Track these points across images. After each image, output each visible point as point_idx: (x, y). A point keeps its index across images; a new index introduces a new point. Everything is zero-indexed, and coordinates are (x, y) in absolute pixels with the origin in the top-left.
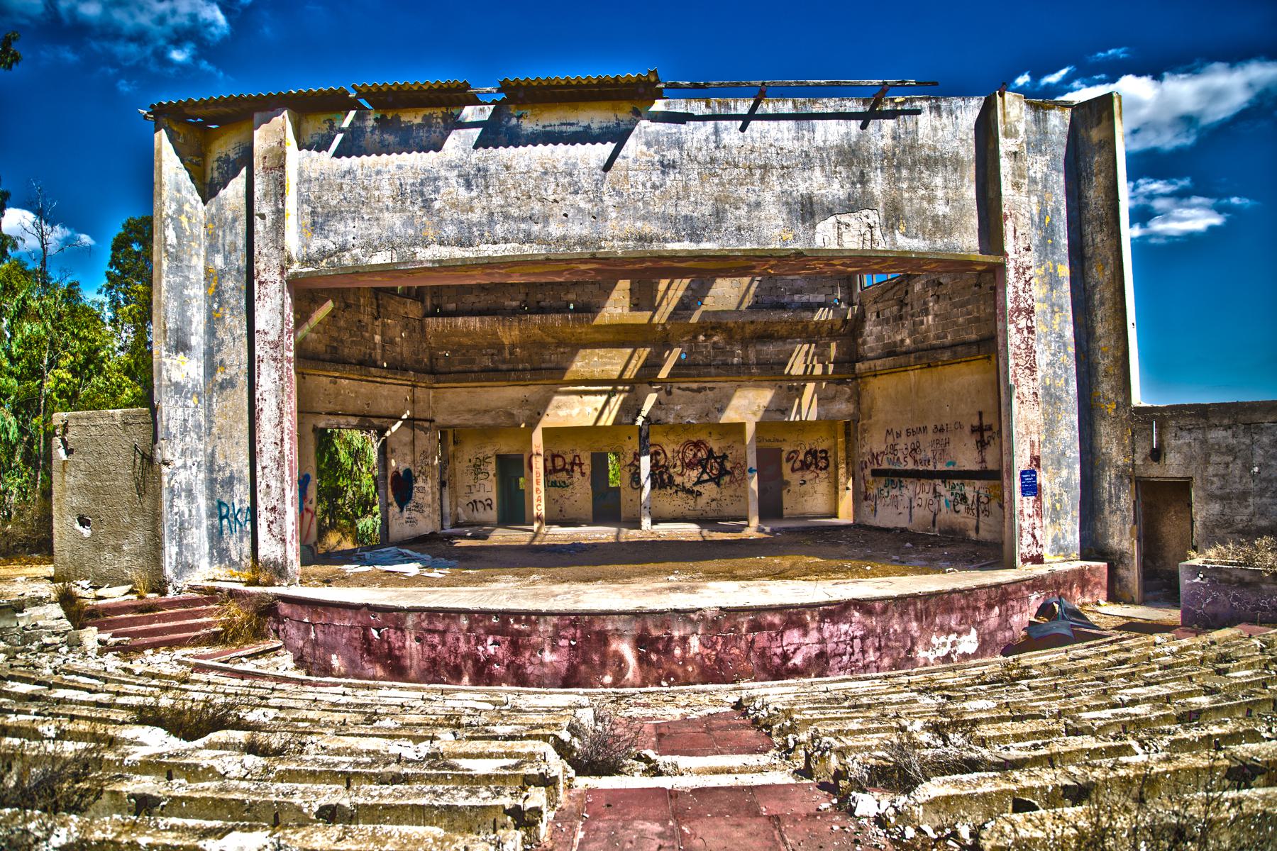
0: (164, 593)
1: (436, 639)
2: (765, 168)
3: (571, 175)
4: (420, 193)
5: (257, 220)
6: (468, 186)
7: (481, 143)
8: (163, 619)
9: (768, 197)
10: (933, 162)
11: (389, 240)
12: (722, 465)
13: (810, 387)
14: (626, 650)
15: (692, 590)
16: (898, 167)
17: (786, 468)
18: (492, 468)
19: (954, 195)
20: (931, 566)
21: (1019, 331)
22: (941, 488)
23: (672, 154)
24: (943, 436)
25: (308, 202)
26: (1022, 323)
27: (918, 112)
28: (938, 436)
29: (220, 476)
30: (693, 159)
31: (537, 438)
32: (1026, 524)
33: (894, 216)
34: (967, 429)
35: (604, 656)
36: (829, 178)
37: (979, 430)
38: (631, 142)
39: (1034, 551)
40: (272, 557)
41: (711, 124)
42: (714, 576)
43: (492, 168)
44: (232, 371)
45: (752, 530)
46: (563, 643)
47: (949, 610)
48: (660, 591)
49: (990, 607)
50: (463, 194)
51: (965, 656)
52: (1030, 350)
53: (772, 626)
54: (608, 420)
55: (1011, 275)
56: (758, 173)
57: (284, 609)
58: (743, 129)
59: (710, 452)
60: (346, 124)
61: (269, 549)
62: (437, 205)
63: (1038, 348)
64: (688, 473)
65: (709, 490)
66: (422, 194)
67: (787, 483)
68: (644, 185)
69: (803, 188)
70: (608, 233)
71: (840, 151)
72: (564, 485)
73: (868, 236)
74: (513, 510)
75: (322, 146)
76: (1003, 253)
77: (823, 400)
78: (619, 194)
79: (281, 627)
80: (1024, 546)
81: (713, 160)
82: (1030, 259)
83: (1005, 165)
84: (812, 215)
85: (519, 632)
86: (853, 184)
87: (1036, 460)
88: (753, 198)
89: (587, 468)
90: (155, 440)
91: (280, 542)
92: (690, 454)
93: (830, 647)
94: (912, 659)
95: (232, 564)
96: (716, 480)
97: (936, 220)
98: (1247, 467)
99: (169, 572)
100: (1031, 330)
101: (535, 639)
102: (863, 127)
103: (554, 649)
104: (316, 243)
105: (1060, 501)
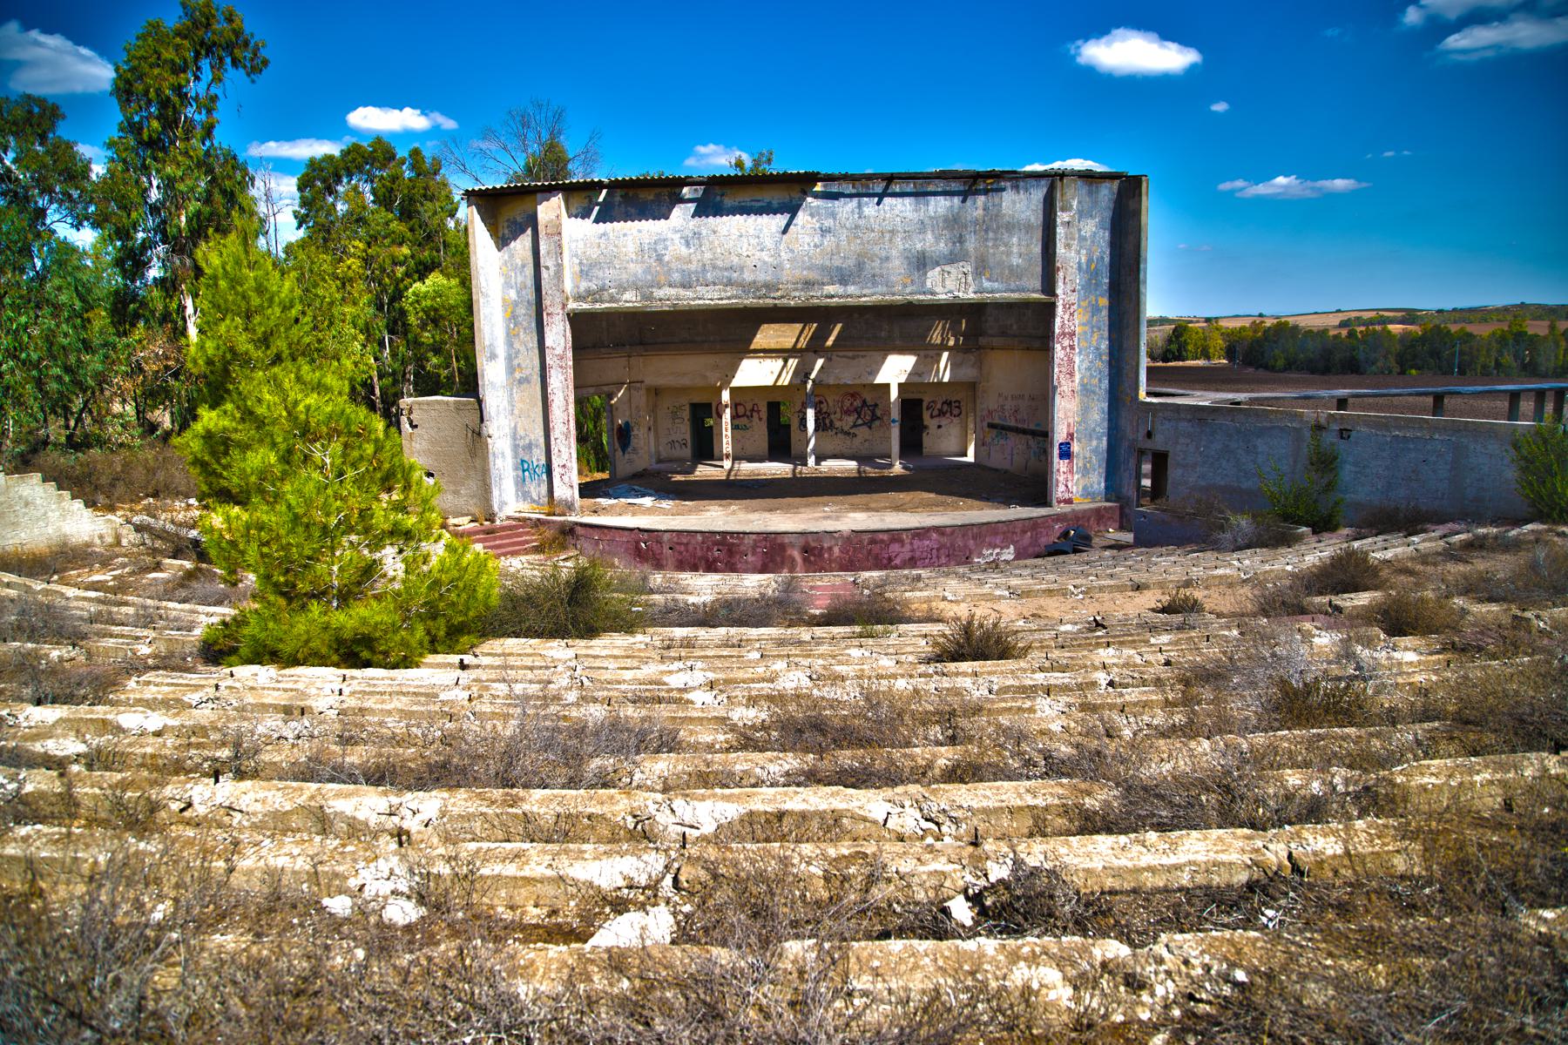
0: (493, 521)
2: (893, 232)
4: (655, 251)
5: (543, 270)
6: (688, 244)
7: (697, 214)
8: (501, 538)
9: (894, 252)
10: (1010, 227)
11: (634, 283)
12: (873, 412)
13: (945, 355)
14: (796, 554)
15: (837, 519)
16: (986, 231)
17: (926, 415)
18: (686, 414)
19: (1021, 250)
20: (1007, 502)
21: (1063, 348)
22: (1031, 442)
23: (828, 223)
25: (576, 256)
26: (1066, 342)
27: (1003, 190)
29: (522, 443)
30: (843, 226)
31: (726, 396)
32: (1061, 479)
33: (981, 268)
35: (783, 558)
36: (937, 239)
38: (800, 214)
39: (1067, 496)
41: (855, 200)
42: (855, 508)
43: (704, 232)
44: (527, 372)
45: (898, 468)
47: (996, 533)
48: (817, 519)
49: (1024, 532)
50: (684, 251)
51: (1007, 562)
52: (1071, 361)
53: (882, 541)
54: (785, 380)
55: (1059, 310)
56: (887, 236)
57: (579, 530)
58: (878, 204)
59: (864, 402)
60: (601, 199)
61: (561, 491)
62: (666, 258)
64: (845, 418)
65: (863, 432)
67: (926, 427)
69: (919, 246)
70: (784, 279)
71: (946, 220)
72: (746, 428)
74: (705, 449)
75: (585, 215)
76: (1055, 295)
77: (955, 365)
78: (792, 251)
80: (1059, 491)
81: (857, 227)
83: (1060, 230)
84: (925, 266)
87: (1071, 435)
88: (884, 254)
89: (764, 414)
90: (482, 420)
91: (567, 485)
92: (847, 403)
93: (918, 554)
95: (533, 501)
96: (869, 425)
97: (1011, 268)
98: (1197, 448)
99: (496, 508)
100: (1072, 347)
101: (742, 548)
102: (964, 201)
104: (584, 285)
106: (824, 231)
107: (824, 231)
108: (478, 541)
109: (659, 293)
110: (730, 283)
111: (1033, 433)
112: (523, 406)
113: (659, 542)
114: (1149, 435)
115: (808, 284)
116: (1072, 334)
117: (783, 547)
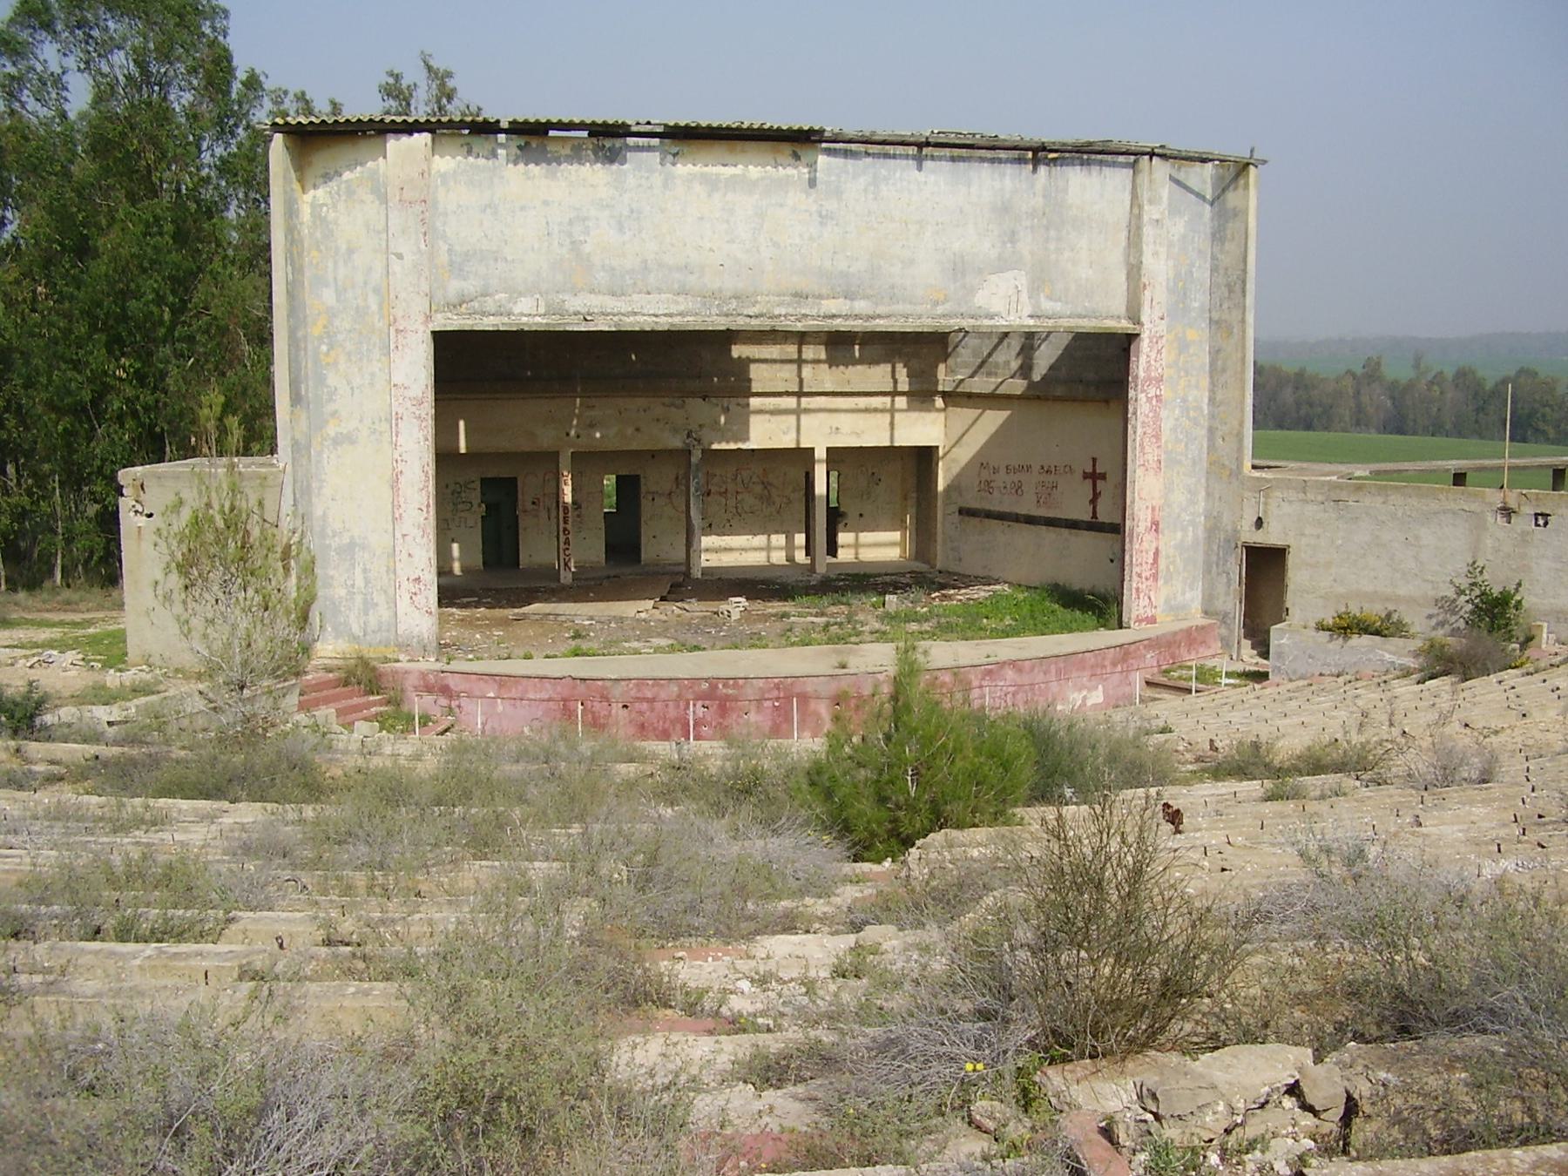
1: (645, 706)
3: (728, 222)
6: (621, 229)
16: (1047, 229)
21: (1149, 400)
24: (1051, 478)
28: (1044, 477)
34: (1078, 475)
37: (1094, 477)
40: (416, 631)
46: (768, 704)
52: (1157, 417)
62: (587, 248)
63: (1164, 414)
66: (570, 235)
68: (801, 236)
73: (1014, 298)
79: (454, 704)
82: (1162, 327)
85: (727, 698)
86: (1004, 243)
94: (1438, 658)
103: (759, 709)
105: (1173, 563)
106: (824, 218)
107: (824, 218)
108: (327, 701)
109: (576, 303)
110: (683, 292)
111: (1094, 526)
112: (359, 471)
113: (605, 698)
114: (1259, 523)
115: (799, 296)
116: (1160, 380)
117: (804, 698)
